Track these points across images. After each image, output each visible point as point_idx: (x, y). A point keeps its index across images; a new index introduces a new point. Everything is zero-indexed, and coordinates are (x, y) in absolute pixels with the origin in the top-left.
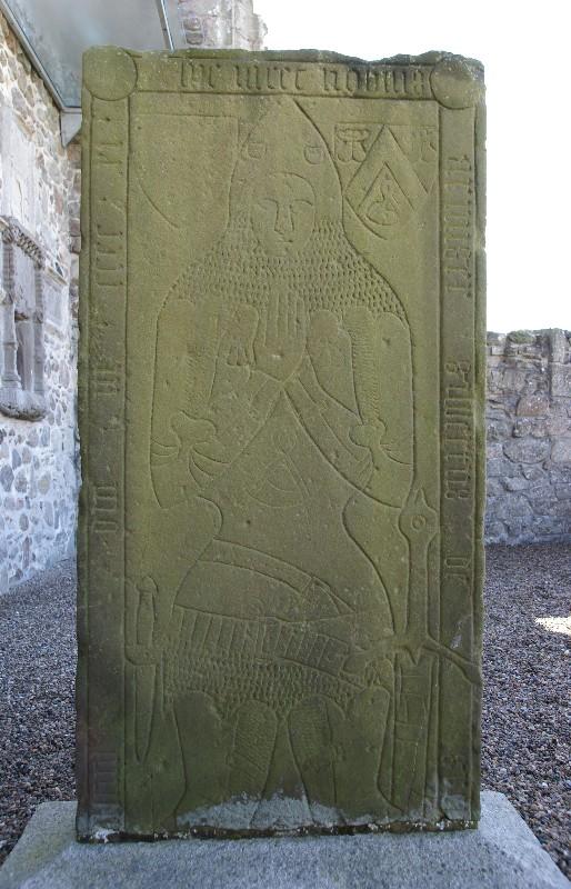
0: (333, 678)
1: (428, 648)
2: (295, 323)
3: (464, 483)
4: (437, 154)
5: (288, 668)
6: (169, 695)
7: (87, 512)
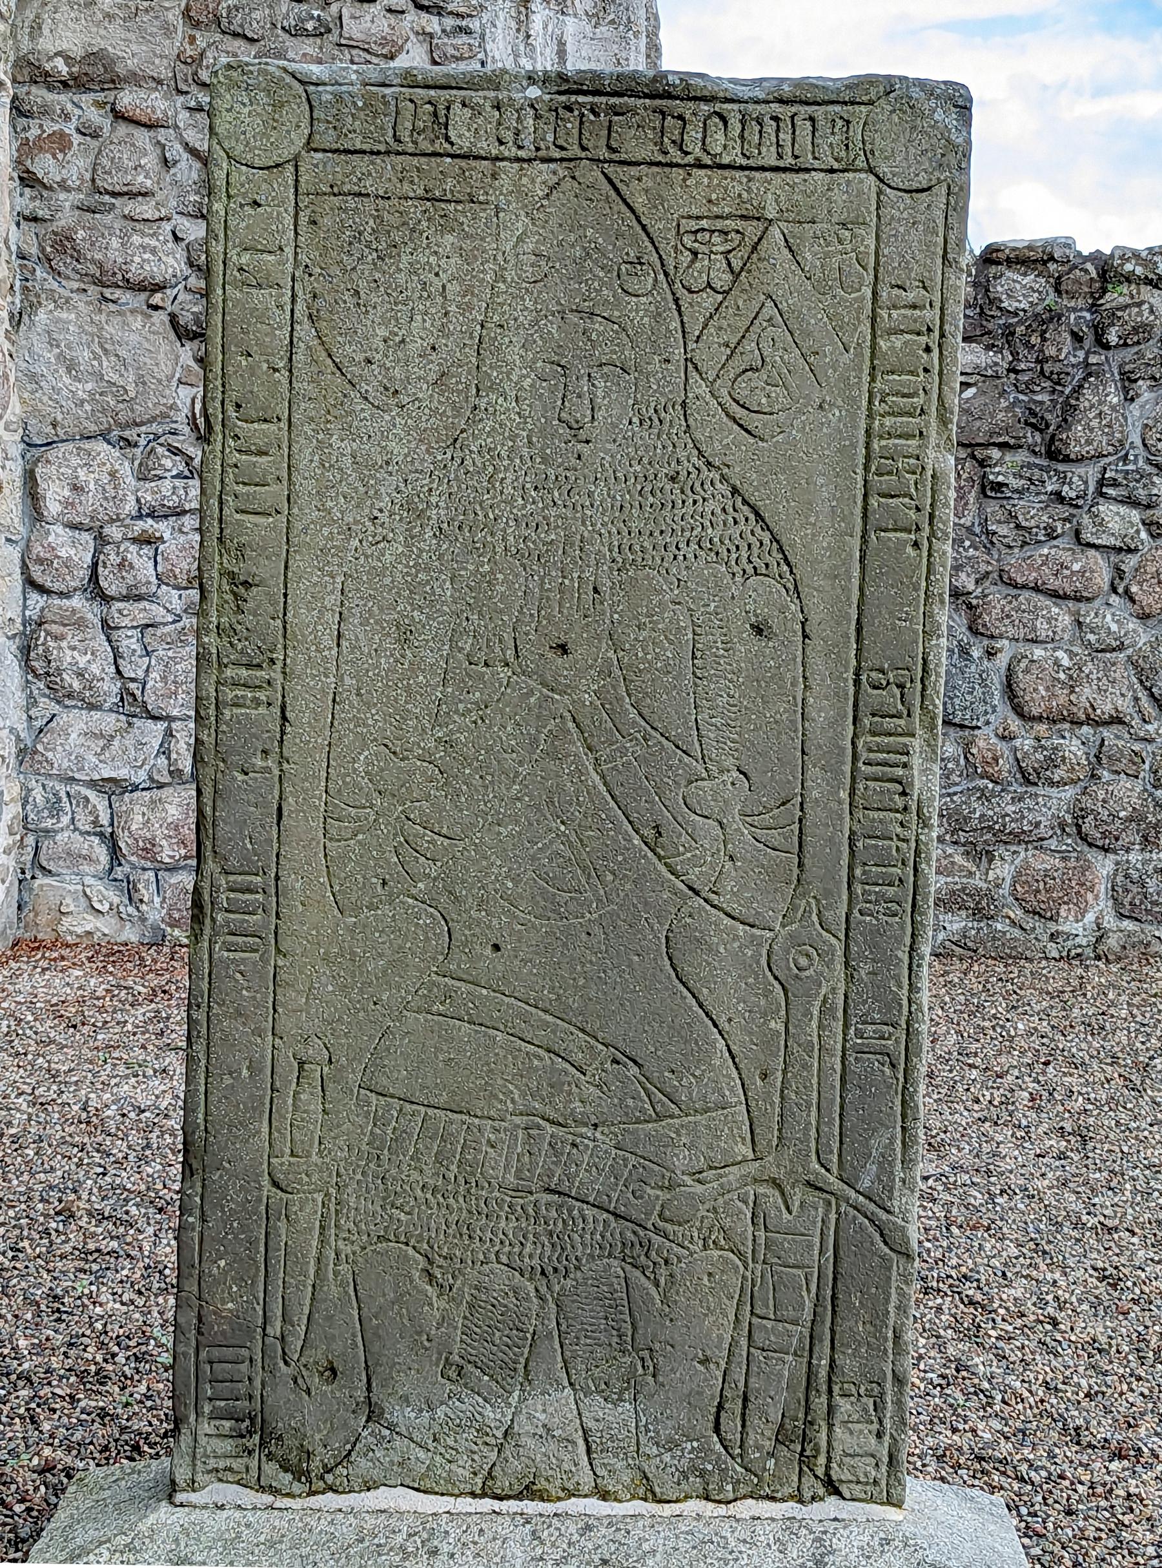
0: (641, 1233)
3: (891, 891)
7: (208, 921)
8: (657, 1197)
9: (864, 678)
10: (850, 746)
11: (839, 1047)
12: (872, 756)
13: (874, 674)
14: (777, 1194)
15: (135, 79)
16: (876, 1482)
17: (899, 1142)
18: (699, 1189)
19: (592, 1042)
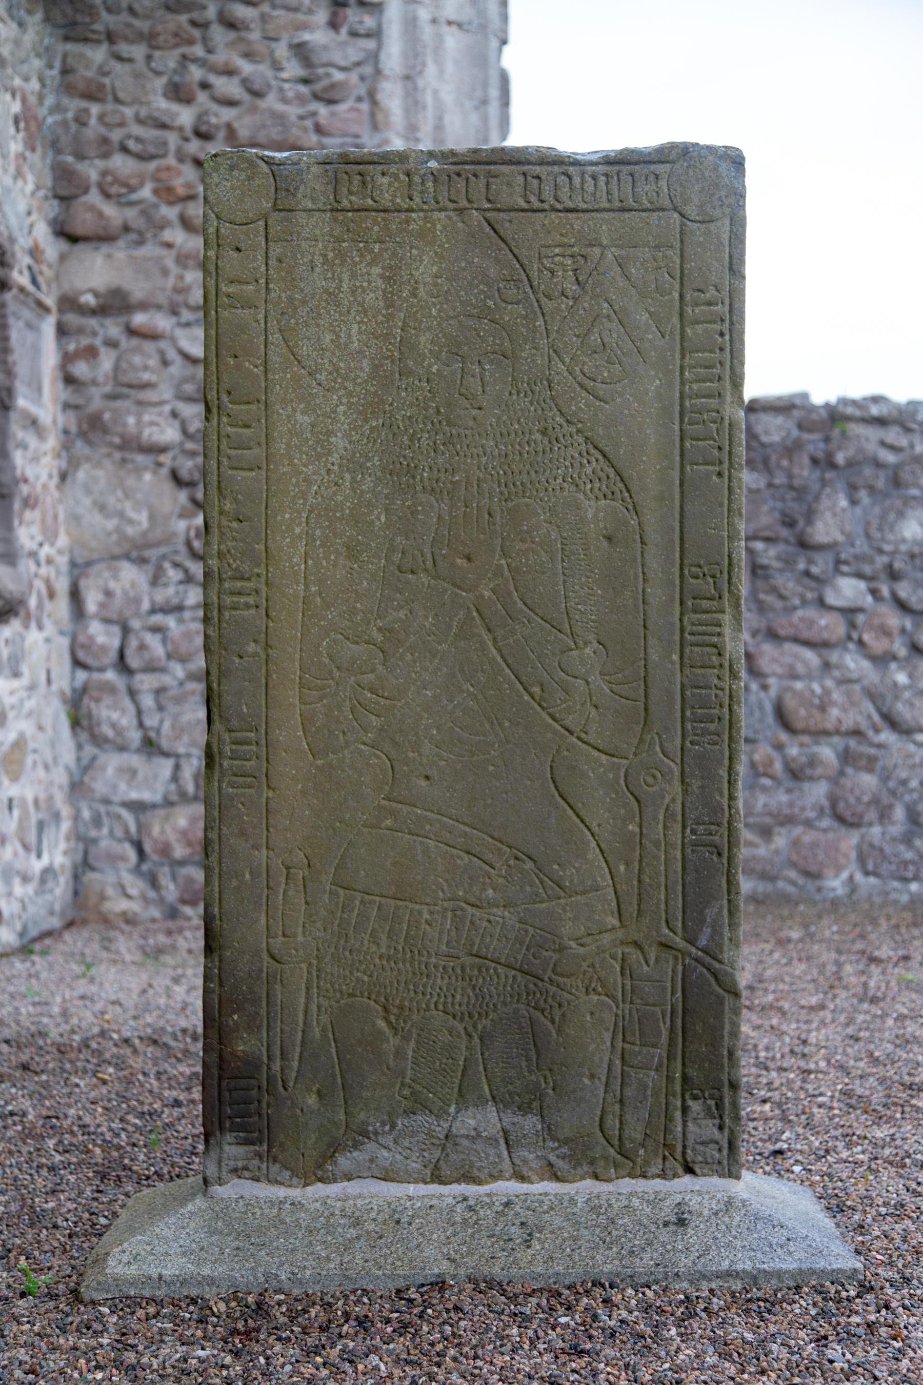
0: (540, 984)
2: (487, 516)
3: (712, 727)
4: (677, 286)
5: (480, 970)
6: (325, 1003)
7: (217, 767)
8: (551, 958)
9: (686, 572)
10: (678, 622)
11: (679, 842)
12: (694, 628)
13: (694, 569)
14: (639, 952)
16: (720, 1163)
17: (725, 911)
18: (582, 950)
19: (499, 845)
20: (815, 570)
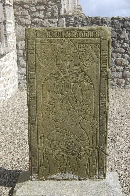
1: (96, 148)
6: (46, 155)
15: (25, 4)
20: (121, 42)
